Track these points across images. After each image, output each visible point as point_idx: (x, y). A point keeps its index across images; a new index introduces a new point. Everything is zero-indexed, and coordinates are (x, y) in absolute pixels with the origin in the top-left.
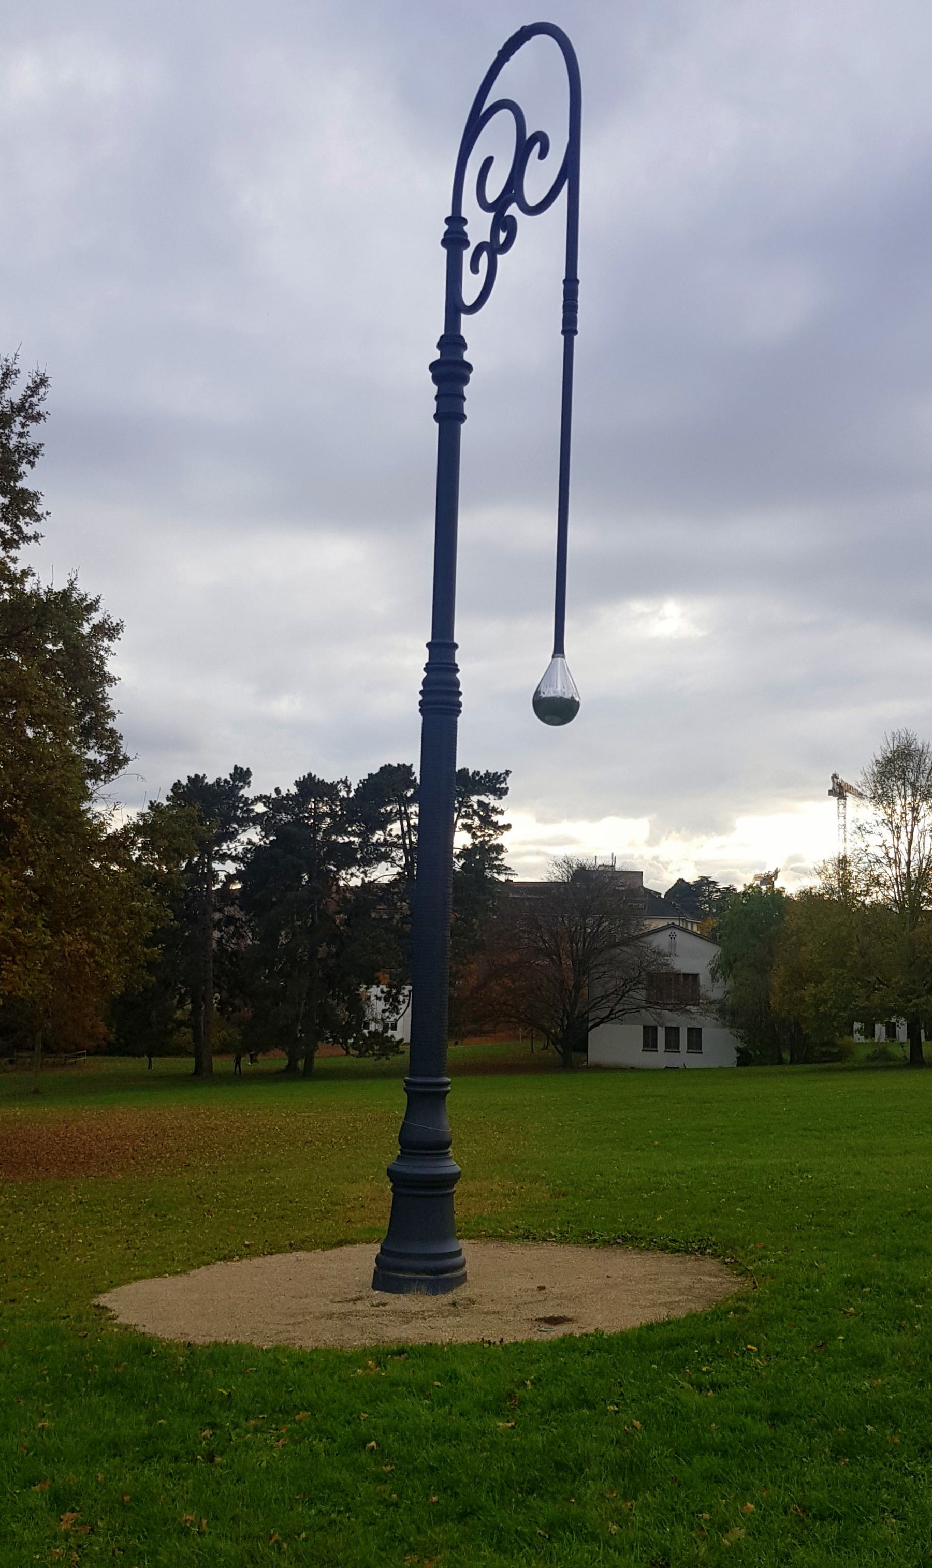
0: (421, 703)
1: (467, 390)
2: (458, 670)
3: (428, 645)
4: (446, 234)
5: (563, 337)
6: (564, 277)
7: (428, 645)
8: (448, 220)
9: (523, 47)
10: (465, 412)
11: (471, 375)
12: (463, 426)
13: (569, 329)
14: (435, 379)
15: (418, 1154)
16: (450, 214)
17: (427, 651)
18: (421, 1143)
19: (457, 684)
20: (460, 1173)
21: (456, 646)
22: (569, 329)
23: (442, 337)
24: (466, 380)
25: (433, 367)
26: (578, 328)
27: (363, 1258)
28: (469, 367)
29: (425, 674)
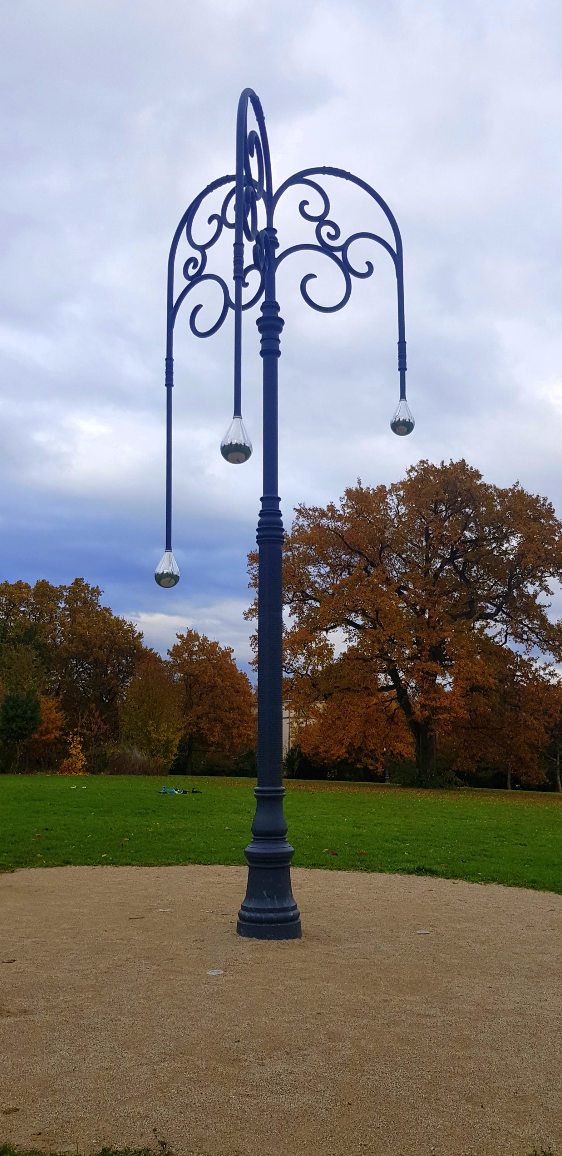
0: (258, 537)
2: (281, 515)
3: (261, 499)
6: (398, 341)
7: (261, 499)
11: (283, 327)
15: (272, 840)
17: (261, 503)
18: (270, 833)
20: (293, 852)
21: (279, 499)
24: (280, 330)
25: (259, 321)
26: (407, 367)
29: (259, 518)
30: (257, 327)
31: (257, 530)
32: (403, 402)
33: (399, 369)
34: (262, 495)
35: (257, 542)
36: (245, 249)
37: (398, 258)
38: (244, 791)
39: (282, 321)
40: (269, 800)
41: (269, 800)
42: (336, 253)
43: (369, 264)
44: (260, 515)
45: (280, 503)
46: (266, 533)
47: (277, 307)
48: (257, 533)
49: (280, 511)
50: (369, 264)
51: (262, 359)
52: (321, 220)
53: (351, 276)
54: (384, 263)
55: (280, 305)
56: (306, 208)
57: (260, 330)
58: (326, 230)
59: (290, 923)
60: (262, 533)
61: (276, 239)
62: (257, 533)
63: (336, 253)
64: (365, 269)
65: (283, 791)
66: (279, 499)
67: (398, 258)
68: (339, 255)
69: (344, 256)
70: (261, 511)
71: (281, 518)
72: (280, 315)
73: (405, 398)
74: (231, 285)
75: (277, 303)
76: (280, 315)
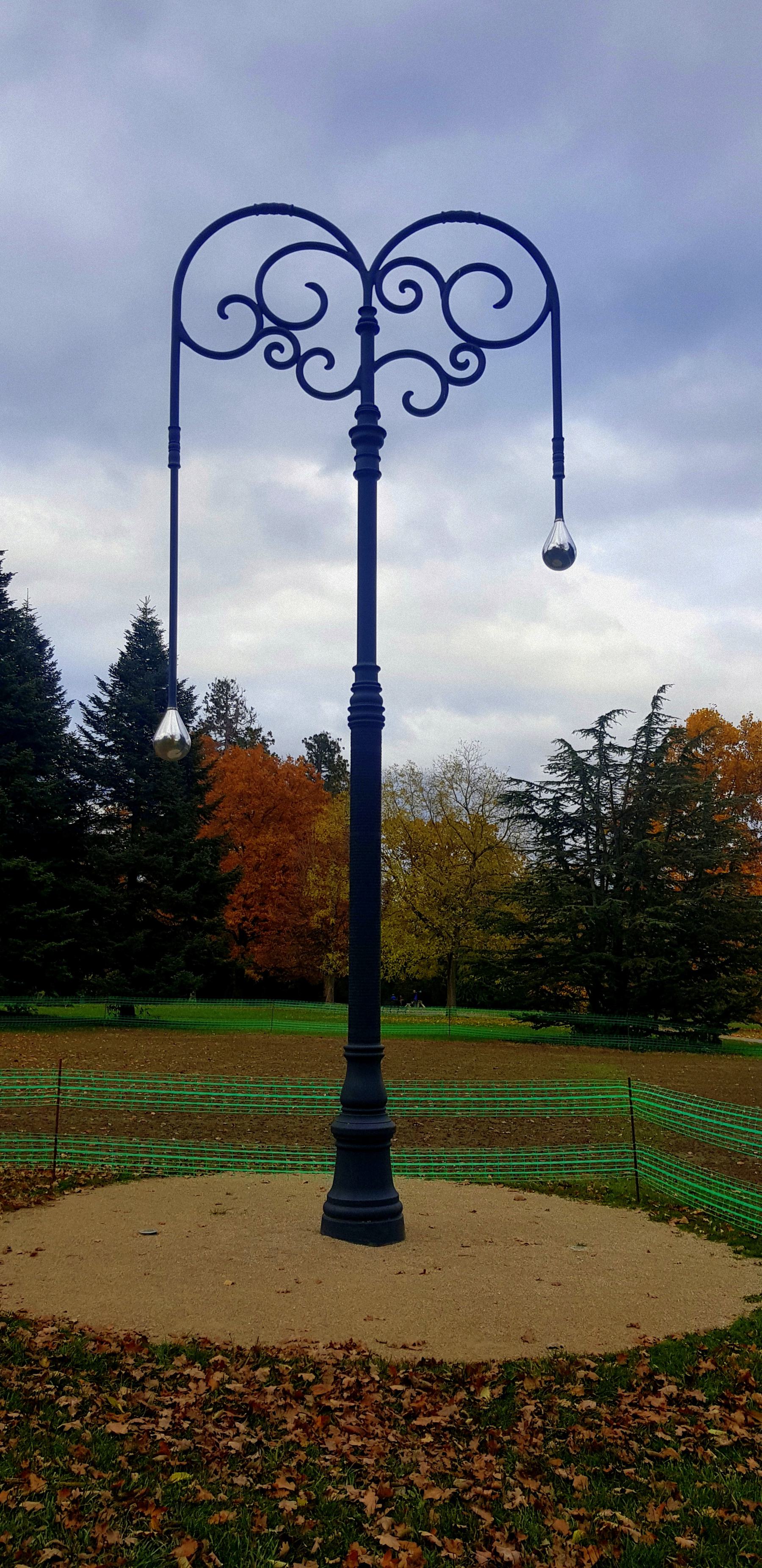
0: (349, 719)
2: (381, 689)
3: (354, 669)
7: (354, 669)
8: (361, 311)
11: (385, 440)
13: (559, 474)
16: (362, 305)
17: (354, 673)
18: (364, 1098)
19: (380, 701)
21: (378, 669)
22: (559, 474)
23: (359, 407)
24: (381, 444)
25: (352, 432)
27: (313, 1185)
29: (352, 694)
30: (350, 439)
31: (349, 709)
32: (560, 524)
33: (554, 477)
34: (355, 663)
35: (349, 725)
36: (181, 432)
37: (179, 335)
38: (331, 1021)
39: (383, 432)
40: (364, 1056)
41: (364, 1056)
42: (272, 325)
43: (224, 316)
44: (352, 690)
45: (379, 673)
46: (360, 713)
47: (376, 414)
48: (349, 714)
49: (379, 685)
50: (224, 316)
51: (356, 482)
52: (299, 360)
53: (254, 298)
54: (200, 323)
55: (380, 410)
56: (322, 360)
57: (354, 443)
58: (288, 353)
59: (389, 1220)
60: (356, 714)
61: (375, 321)
62: (349, 714)
63: (272, 325)
64: (228, 309)
65: (381, 1049)
66: (378, 669)
67: (179, 335)
68: (268, 323)
69: (260, 322)
70: (354, 685)
71: (381, 694)
72: (381, 423)
73: (562, 517)
74: (376, 302)
75: (376, 407)
76: (381, 423)
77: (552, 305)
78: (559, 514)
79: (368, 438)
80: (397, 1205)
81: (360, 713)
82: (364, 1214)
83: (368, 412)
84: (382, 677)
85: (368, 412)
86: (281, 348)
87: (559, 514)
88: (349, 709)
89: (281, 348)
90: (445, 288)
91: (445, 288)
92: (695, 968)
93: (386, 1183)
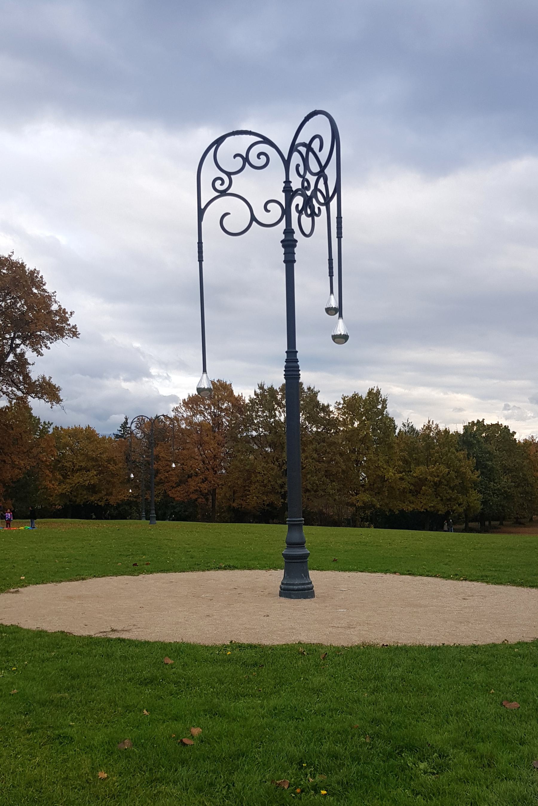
1: (296, 250)
3: (286, 352)
4: (284, 188)
5: (337, 239)
8: (284, 182)
9: (314, 117)
10: (296, 259)
12: (295, 264)
14: (283, 246)
16: (285, 180)
23: (285, 230)
24: (295, 246)
25: (282, 242)
27: (277, 576)
28: (296, 241)
31: (285, 371)
32: (205, 375)
34: (286, 350)
46: (289, 373)
53: (228, 192)
73: (206, 372)
77: (201, 212)
78: (205, 371)
79: (289, 244)
80: (311, 585)
81: (289, 373)
82: (296, 588)
83: (289, 231)
84: (298, 356)
85: (289, 231)
86: (222, 184)
87: (205, 371)
88: (285, 371)
89: (222, 184)
90: (253, 218)
91: (253, 218)
92: (423, 487)
93: (307, 576)
